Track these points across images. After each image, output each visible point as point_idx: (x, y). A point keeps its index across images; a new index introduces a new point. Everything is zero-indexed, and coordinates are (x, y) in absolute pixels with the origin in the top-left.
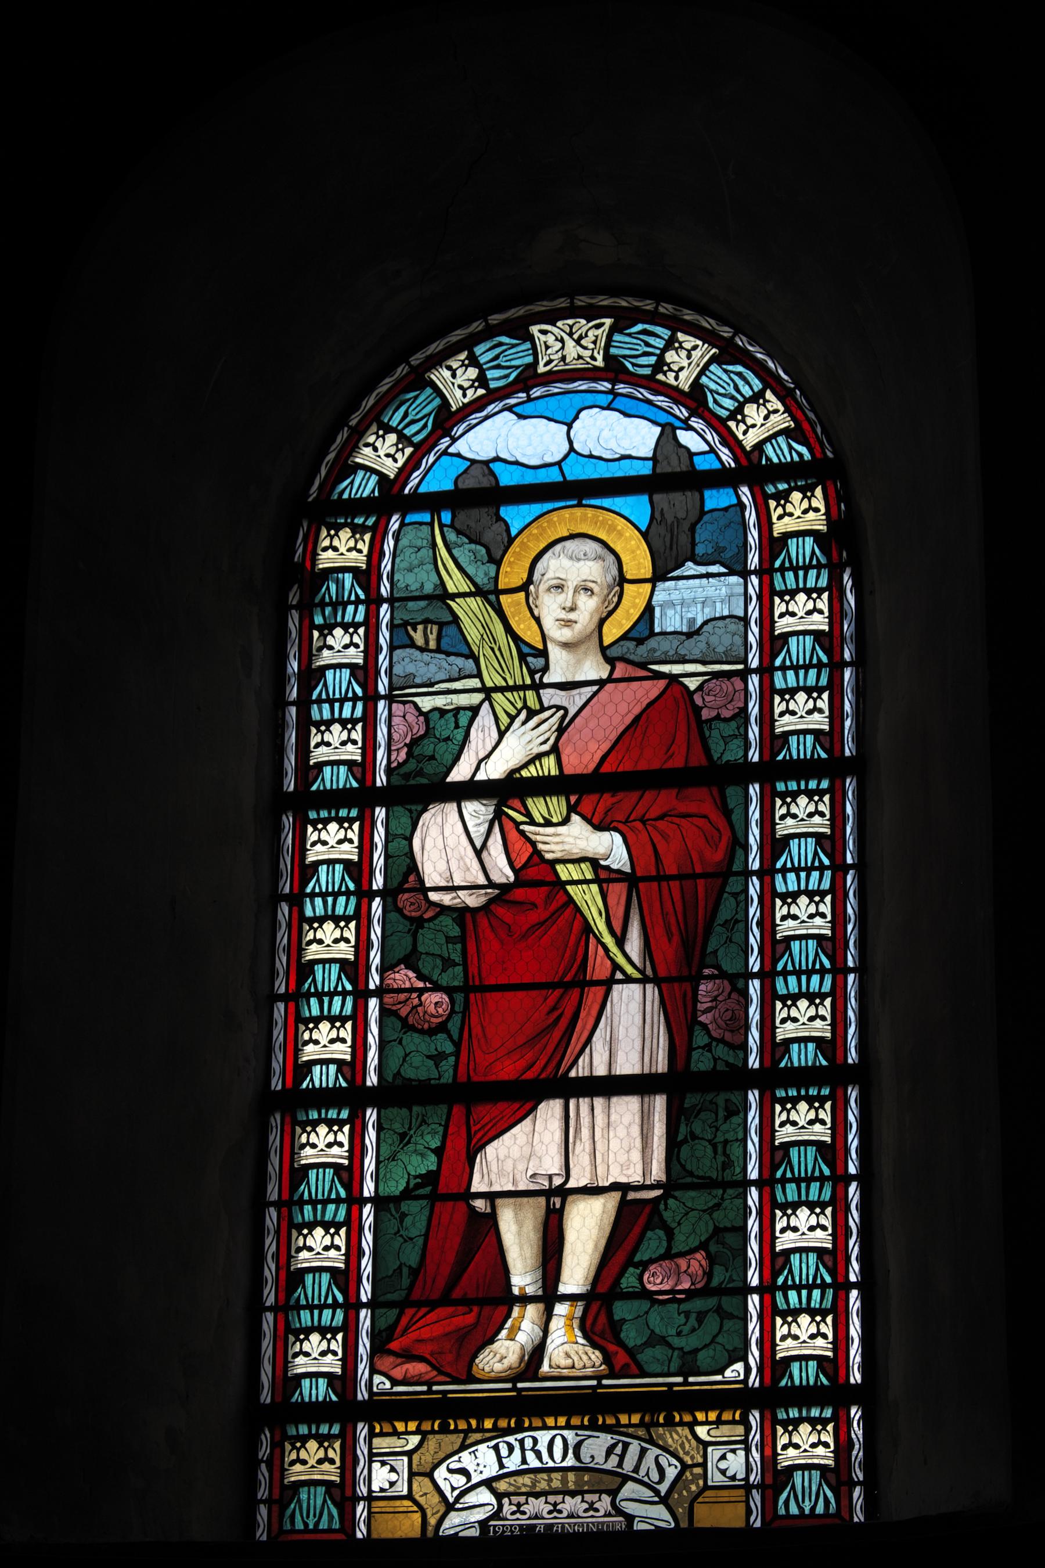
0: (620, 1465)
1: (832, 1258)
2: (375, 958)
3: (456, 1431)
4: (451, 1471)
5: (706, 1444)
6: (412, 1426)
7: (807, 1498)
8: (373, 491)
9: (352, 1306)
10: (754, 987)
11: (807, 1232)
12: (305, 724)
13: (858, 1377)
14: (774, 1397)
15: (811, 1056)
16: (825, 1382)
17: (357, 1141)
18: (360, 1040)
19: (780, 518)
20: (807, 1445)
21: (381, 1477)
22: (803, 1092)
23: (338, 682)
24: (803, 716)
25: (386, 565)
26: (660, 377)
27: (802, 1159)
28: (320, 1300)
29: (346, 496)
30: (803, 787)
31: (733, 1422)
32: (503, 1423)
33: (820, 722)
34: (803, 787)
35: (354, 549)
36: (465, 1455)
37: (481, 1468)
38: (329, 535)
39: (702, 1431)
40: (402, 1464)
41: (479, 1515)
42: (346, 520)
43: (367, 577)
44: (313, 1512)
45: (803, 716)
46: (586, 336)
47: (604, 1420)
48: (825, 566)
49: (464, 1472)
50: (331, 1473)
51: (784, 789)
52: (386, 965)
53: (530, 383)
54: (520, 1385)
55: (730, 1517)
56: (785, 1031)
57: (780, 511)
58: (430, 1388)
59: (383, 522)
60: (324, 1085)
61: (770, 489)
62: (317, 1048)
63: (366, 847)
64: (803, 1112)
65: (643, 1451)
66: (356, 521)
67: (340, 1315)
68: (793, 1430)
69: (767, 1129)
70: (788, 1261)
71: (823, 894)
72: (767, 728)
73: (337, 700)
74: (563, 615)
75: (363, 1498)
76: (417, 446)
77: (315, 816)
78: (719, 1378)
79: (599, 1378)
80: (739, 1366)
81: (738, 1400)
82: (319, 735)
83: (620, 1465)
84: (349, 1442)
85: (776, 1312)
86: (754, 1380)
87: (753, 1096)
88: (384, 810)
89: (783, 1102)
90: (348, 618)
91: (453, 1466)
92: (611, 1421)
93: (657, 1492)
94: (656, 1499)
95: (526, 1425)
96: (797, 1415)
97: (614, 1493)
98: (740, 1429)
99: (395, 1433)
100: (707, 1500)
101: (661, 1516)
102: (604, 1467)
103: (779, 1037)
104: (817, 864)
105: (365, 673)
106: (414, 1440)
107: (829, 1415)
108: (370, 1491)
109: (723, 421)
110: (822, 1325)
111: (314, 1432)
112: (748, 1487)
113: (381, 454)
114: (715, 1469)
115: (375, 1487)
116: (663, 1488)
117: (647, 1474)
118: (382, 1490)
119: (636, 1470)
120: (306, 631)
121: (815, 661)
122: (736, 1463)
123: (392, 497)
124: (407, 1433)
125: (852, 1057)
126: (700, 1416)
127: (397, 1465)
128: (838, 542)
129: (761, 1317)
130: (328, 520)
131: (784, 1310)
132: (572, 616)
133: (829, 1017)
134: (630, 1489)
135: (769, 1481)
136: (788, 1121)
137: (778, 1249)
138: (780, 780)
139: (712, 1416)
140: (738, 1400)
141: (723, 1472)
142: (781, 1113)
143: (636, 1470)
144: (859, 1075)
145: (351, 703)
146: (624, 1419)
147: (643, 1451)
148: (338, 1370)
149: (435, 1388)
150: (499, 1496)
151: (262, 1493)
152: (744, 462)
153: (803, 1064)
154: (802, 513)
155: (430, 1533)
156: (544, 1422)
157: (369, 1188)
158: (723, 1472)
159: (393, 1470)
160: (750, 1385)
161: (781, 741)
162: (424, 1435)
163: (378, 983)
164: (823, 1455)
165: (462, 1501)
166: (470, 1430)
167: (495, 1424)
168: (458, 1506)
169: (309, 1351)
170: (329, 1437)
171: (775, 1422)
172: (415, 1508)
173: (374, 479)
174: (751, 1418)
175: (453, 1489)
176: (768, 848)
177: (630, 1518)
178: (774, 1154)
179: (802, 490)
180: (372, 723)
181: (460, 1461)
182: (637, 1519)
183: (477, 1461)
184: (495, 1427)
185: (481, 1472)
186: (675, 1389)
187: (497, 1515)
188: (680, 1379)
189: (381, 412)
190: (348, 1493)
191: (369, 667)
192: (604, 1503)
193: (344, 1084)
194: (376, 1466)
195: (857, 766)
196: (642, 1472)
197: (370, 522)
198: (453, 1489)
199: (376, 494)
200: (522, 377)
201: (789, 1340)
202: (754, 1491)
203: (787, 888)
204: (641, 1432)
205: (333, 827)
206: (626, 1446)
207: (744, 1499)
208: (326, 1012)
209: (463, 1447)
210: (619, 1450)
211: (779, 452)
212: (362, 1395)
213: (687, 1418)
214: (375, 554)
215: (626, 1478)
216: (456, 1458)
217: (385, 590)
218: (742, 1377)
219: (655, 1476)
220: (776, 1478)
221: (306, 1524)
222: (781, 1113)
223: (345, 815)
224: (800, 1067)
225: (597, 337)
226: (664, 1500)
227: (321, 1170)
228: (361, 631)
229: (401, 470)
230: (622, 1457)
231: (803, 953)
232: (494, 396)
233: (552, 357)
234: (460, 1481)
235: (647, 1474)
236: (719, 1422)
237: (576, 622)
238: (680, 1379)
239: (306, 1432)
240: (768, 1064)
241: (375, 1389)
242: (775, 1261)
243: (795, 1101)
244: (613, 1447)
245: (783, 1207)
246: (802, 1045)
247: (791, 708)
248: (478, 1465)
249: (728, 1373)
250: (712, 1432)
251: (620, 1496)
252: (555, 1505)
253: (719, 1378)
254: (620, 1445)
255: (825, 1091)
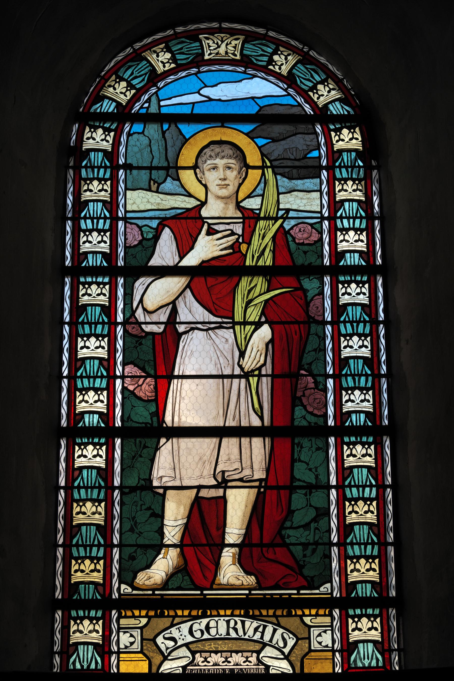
0: (262, 637)
1: (378, 528)
2: (120, 359)
3: (168, 616)
4: (165, 638)
5: (310, 627)
6: (144, 613)
7: (367, 657)
8: (114, 110)
9: (109, 546)
10: (330, 383)
11: (367, 631)
12: (77, 231)
13: (387, 422)
14: (348, 603)
15: (357, 261)
16: (370, 424)
17: (112, 346)
18: (110, 456)
19: (337, 141)
20: (366, 630)
21: (125, 639)
22: (359, 439)
23: (96, 209)
24: (352, 242)
25: (122, 149)
26: (271, 67)
27: (356, 366)
28: (90, 542)
29: (98, 111)
30: (364, 612)
31: (325, 615)
32: (194, 613)
33: (368, 406)
34: (364, 612)
35: (104, 140)
36: (173, 629)
37: (183, 637)
38: (90, 131)
39: (307, 620)
40: (137, 633)
41: (184, 662)
42: (100, 124)
43: (111, 155)
44: (86, 659)
45: (352, 242)
46: (230, 43)
47: (253, 613)
48: (364, 218)
49: (173, 639)
50: (96, 638)
51: (348, 441)
52: (126, 361)
53: (200, 64)
54: (205, 592)
55: (324, 668)
56: (348, 407)
57: (337, 138)
58: (154, 592)
59: (121, 126)
60: (95, 265)
61: (332, 127)
62: (90, 298)
63: (112, 350)
64: (365, 623)
65: (275, 631)
66: (105, 125)
67: (105, 382)
68: (356, 562)
69: (340, 459)
70: (352, 472)
71: (371, 500)
72: (340, 464)
73: (93, 323)
74: (220, 182)
75: (115, 652)
76: (138, 90)
77: (80, 441)
78: (317, 591)
79: (250, 590)
80: (328, 585)
81: (327, 604)
82: (80, 451)
83: (262, 637)
84: (107, 621)
85: (348, 557)
86: (336, 594)
87: (332, 440)
88: (122, 279)
89: (343, 283)
90: (101, 175)
91: (167, 636)
92: (257, 613)
93: (283, 653)
94: (282, 657)
95: (209, 613)
96: (360, 613)
97: (258, 652)
98: (328, 619)
99: (134, 616)
100: (310, 657)
101: (284, 666)
102: (253, 638)
103: (337, 199)
104: (368, 483)
105: (112, 205)
106: (144, 621)
107: (371, 441)
108: (119, 648)
109: (306, 92)
110: (373, 564)
111: (86, 615)
112: (333, 651)
113: (119, 92)
114: (315, 641)
115: (122, 646)
116: (286, 651)
117: (277, 643)
118: (126, 647)
119: (271, 641)
120: (77, 182)
121: (359, 215)
122: (327, 639)
123: (124, 114)
124: (140, 616)
125: (379, 261)
126: (307, 612)
127: (134, 634)
128: (371, 153)
129: (329, 232)
130: (90, 123)
131: (350, 498)
132: (226, 182)
133: (377, 569)
134: (268, 651)
135: (345, 648)
136: (353, 511)
137: (344, 411)
138: (346, 436)
139: (313, 612)
140: (327, 604)
141: (320, 643)
142: (344, 342)
143: (271, 641)
144: (383, 270)
145: (100, 379)
146: (264, 612)
147: (275, 631)
148: (103, 466)
149: (157, 592)
150: (193, 653)
151: (57, 648)
152: (318, 112)
153: (353, 264)
154: (348, 140)
155: (154, 670)
156: (218, 613)
157: (117, 482)
158: (320, 643)
159: (132, 636)
160: (334, 595)
161: (339, 205)
162: (150, 618)
163: (124, 162)
164: (371, 518)
165: (172, 655)
166: (176, 616)
167: (190, 613)
168: (169, 658)
169: (84, 569)
170: (105, 284)
171: (343, 443)
172: (145, 659)
173: (114, 104)
174: (334, 613)
175: (167, 648)
176: (342, 529)
177: (267, 667)
178: (344, 472)
179: (349, 128)
180: (111, 474)
181: (171, 633)
182: (271, 667)
183: (181, 633)
184: (190, 615)
185: (183, 639)
186: (292, 596)
187: (191, 663)
188: (295, 592)
189: (119, 70)
190: (107, 649)
191: (113, 202)
192: (253, 659)
193: (99, 597)
194: (121, 634)
195: (383, 270)
196: (274, 642)
197: (113, 127)
198: (167, 648)
199: (115, 111)
200: (195, 60)
201: (348, 348)
202: (337, 654)
203: (354, 553)
204: (274, 620)
205: (90, 447)
206: (265, 627)
207: (331, 657)
208: (93, 332)
209: (172, 625)
210: (261, 629)
211: (337, 109)
212: (115, 595)
213: (299, 612)
214: (116, 143)
215: (265, 645)
216: (169, 631)
217: (121, 161)
218: (329, 591)
219: (281, 644)
220: (348, 648)
221: (82, 666)
222: (344, 342)
223: (101, 281)
224: (351, 265)
225: (236, 45)
226: (287, 658)
227: (94, 307)
228: (108, 234)
229: (129, 101)
230: (263, 633)
231: (361, 533)
232: (179, 68)
233: (212, 52)
234: (171, 644)
235: (277, 643)
236: (317, 615)
237: (229, 185)
238: (295, 592)
239: (82, 615)
240: (339, 424)
241: (122, 592)
242: (346, 529)
243: (349, 283)
244: (258, 627)
245: (346, 390)
246: (356, 360)
247: (359, 626)
248: (181, 635)
249: (322, 589)
250: (312, 621)
251: (261, 655)
252: (226, 658)
253: (317, 591)
254: (262, 627)
255: (365, 278)
